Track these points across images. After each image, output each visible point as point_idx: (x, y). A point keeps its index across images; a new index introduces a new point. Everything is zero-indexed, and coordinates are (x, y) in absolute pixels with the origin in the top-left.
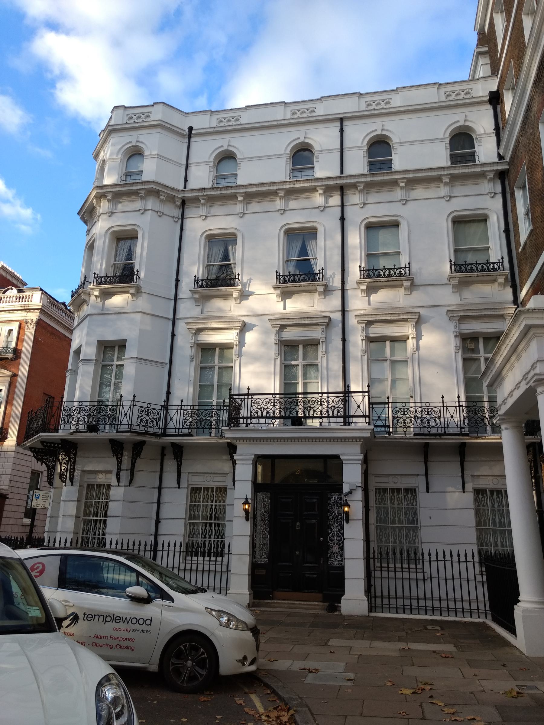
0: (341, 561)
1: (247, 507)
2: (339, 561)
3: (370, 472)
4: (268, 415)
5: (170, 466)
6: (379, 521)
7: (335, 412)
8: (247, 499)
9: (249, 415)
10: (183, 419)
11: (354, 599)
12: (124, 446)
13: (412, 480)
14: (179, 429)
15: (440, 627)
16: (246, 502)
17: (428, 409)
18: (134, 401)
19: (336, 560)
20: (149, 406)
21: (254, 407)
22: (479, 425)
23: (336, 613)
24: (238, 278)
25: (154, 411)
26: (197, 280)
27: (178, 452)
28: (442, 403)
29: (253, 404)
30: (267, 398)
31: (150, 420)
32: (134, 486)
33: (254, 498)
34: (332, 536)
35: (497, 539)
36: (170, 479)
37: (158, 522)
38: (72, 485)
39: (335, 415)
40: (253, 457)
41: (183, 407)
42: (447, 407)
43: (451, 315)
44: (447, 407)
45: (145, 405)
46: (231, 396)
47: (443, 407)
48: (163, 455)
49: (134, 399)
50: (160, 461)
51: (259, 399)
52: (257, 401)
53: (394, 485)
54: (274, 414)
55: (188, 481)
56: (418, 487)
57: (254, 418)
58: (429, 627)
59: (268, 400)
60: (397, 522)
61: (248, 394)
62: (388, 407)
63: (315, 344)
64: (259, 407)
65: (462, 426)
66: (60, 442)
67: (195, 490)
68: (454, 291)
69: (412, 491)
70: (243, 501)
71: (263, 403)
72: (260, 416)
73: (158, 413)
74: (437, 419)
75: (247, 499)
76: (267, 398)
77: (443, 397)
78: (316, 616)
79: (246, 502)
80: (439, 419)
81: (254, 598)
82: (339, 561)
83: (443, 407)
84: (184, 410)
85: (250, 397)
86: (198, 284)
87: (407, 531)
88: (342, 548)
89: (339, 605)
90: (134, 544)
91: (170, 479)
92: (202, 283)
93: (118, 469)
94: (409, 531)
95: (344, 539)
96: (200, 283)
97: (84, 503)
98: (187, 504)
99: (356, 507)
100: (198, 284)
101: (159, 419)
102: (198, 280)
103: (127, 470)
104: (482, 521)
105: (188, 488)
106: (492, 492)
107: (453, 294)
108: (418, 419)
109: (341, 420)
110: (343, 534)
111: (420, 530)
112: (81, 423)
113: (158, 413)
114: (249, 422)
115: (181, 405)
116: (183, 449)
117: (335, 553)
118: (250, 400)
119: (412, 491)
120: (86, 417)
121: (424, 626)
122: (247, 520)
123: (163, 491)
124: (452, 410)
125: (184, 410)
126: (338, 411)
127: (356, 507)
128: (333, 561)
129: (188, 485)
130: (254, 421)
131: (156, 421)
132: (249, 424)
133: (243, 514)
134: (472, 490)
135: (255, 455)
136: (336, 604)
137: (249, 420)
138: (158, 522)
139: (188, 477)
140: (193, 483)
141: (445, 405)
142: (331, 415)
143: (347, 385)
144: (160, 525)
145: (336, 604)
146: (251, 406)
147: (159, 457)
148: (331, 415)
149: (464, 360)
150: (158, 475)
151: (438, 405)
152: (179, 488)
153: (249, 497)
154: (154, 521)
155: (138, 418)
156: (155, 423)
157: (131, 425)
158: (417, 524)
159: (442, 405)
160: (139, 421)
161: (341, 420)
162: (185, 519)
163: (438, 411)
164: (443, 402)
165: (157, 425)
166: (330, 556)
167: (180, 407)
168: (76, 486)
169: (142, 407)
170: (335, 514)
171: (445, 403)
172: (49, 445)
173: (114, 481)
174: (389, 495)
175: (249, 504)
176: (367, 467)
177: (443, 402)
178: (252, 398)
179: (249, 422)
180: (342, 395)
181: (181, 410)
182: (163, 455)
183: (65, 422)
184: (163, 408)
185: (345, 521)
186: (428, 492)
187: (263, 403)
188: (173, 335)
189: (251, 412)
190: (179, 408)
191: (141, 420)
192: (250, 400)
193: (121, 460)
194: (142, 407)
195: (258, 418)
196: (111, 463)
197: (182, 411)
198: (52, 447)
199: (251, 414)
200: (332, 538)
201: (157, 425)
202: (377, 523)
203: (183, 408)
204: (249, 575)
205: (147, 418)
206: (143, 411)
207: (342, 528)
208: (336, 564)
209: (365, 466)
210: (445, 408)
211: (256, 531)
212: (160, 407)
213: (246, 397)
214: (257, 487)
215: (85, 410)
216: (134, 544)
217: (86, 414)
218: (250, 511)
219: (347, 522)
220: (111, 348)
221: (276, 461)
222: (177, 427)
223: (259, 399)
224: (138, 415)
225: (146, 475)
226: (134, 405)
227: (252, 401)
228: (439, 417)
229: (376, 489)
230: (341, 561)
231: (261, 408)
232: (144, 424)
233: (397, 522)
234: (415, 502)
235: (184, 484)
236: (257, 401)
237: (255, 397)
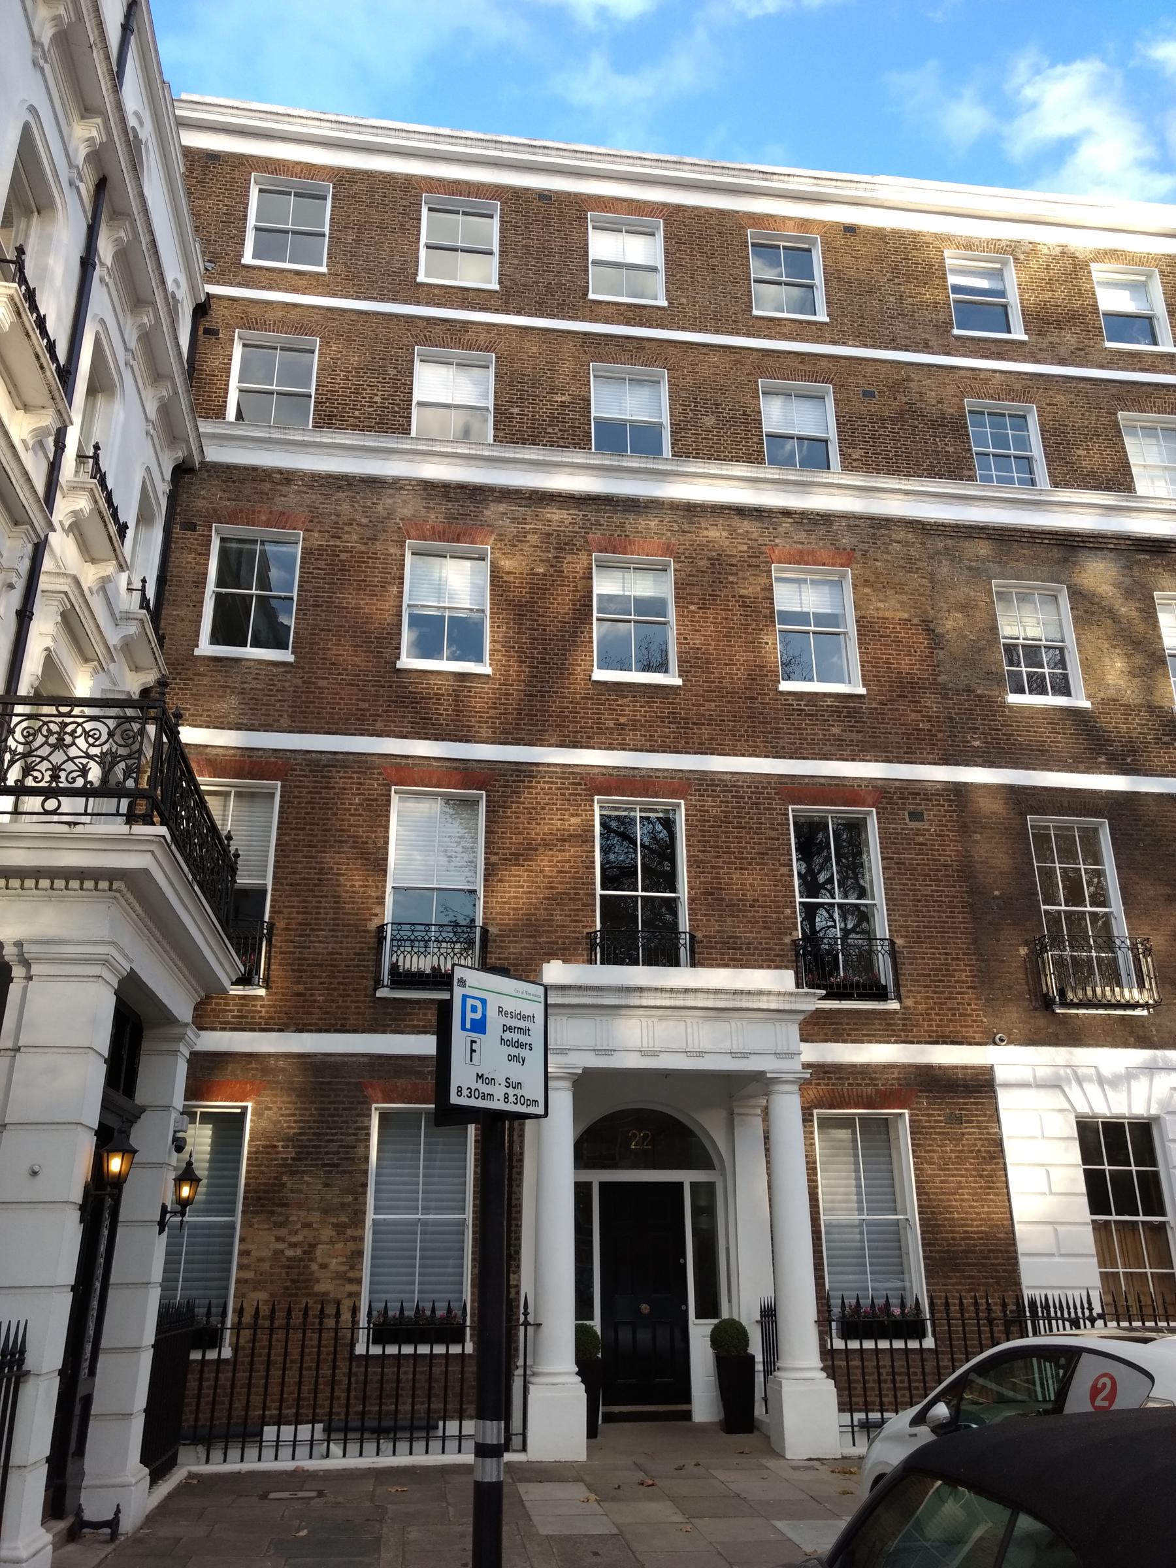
4: (29, 782)
54: (55, 777)
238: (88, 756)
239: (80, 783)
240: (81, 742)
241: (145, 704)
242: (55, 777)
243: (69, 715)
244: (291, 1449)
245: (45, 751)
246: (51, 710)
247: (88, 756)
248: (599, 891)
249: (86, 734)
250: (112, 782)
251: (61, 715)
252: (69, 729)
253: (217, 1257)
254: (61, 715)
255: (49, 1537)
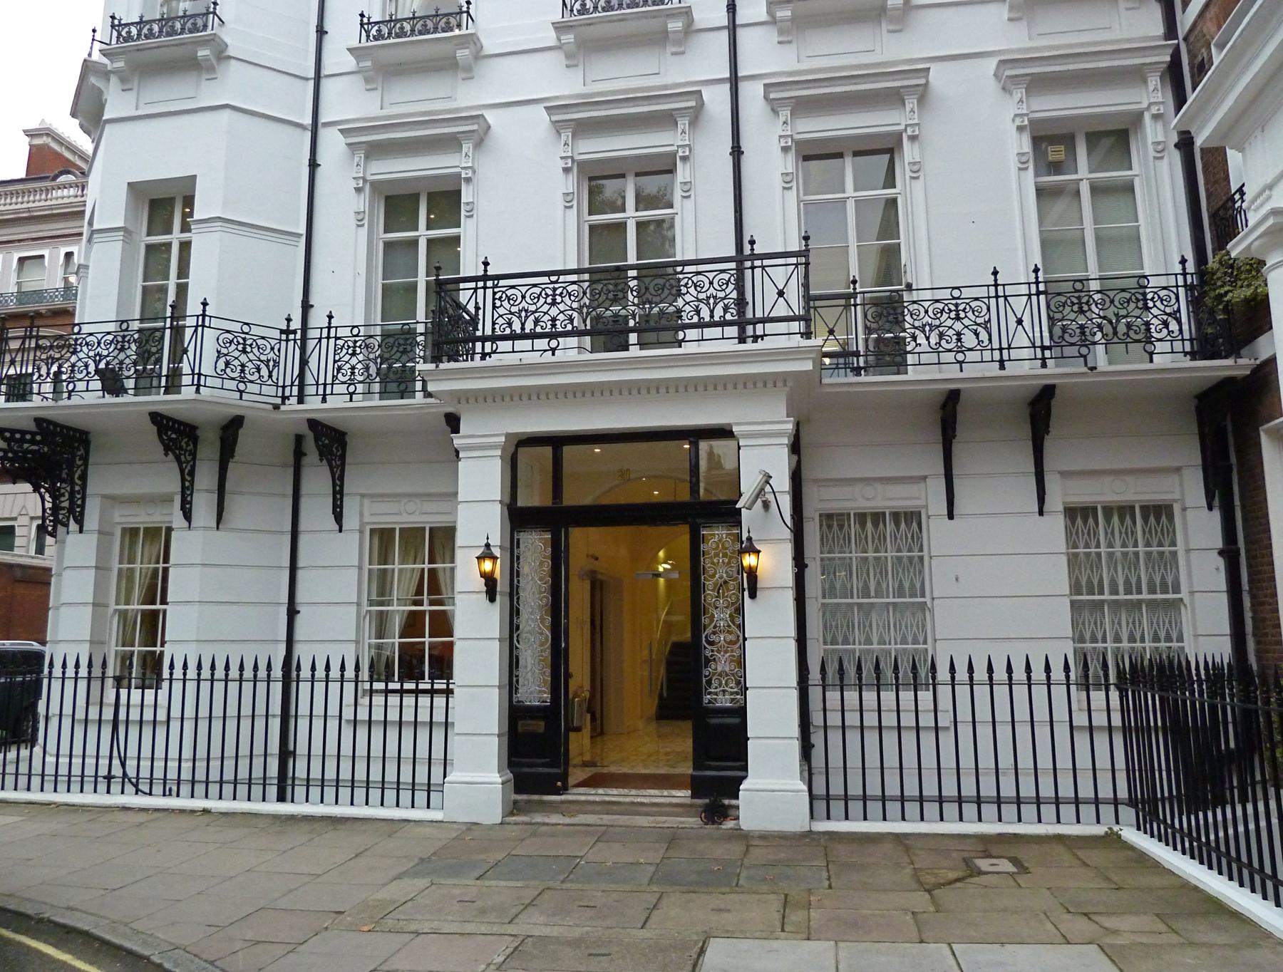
0: (737, 693)
1: (487, 566)
2: (732, 693)
3: (806, 475)
4: (538, 329)
5: (317, 481)
6: (829, 591)
7: (719, 312)
8: (488, 546)
9: (488, 332)
10: (335, 362)
11: (772, 788)
12: (199, 433)
13: (912, 490)
14: (325, 385)
15: (1015, 861)
16: (487, 554)
17: (957, 305)
18: (204, 315)
19: (724, 691)
20: (246, 329)
21: (501, 311)
22: (1090, 338)
23: (729, 824)
24: (468, 12)
25: (260, 342)
26: (365, 23)
27: (329, 443)
28: (992, 289)
29: (498, 303)
30: (535, 285)
31: (250, 365)
32: (226, 530)
33: (513, 547)
34: (714, 633)
35: (1120, 624)
36: (316, 510)
37: (292, 612)
38: (81, 531)
39: (716, 318)
40: (503, 439)
41: (333, 331)
42: (1005, 297)
43: (1008, 73)
44: (1005, 297)
45: (236, 327)
46: (443, 290)
47: (997, 297)
48: (299, 454)
49: (204, 310)
50: (292, 470)
51: (513, 287)
52: (509, 293)
53: (868, 504)
54: (554, 326)
55: (361, 515)
56: (926, 507)
57: (504, 338)
58: (984, 864)
59: (537, 290)
60: (873, 594)
61: (485, 278)
62: (855, 305)
63: (665, 166)
64: (514, 309)
65: (1047, 343)
66: (32, 426)
67: (383, 537)
68: (1013, 15)
69: (911, 518)
70: (479, 552)
71: (523, 297)
72: (519, 331)
73: (272, 349)
74: (980, 329)
75: (488, 546)
76: (535, 285)
77: (995, 273)
78: (672, 839)
79: (487, 554)
80: (986, 328)
81: (518, 790)
82: (732, 693)
83: (997, 297)
84: (337, 338)
85: (490, 284)
86: (368, 32)
87: (898, 615)
88: (741, 662)
89: (734, 802)
90: (213, 667)
91: (316, 510)
92: (379, 31)
93: (184, 488)
94: (868, 614)
95: (745, 639)
96: (374, 32)
97: (115, 572)
98: (360, 568)
99: (772, 562)
100: (368, 32)
101: (276, 364)
102: (369, 23)
103: (207, 491)
104: (1096, 584)
105: (361, 532)
106: (1108, 511)
107: (1012, 24)
108: (931, 330)
109: (733, 331)
110: (742, 627)
111: (932, 611)
112: (79, 376)
113: (272, 349)
114: (488, 350)
115: (329, 328)
116: (348, 439)
117: (720, 675)
118: (489, 292)
119: (911, 518)
120: (91, 362)
121: (964, 860)
122: (492, 599)
123: (303, 540)
124: (1019, 304)
125: (337, 338)
126: (726, 309)
127: (772, 562)
128: (716, 694)
129: (362, 524)
130: (504, 345)
131: (268, 366)
132: (489, 354)
133: (480, 584)
134: (1061, 509)
135: (508, 435)
136: (726, 802)
137: (488, 345)
138: (292, 612)
139: (362, 505)
140: (374, 519)
141: (1001, 293)
142: (707, 319)
143: (746, 239)
144: (300, 620)
145: (726, 802)
146: (494, 307)
147: (291, 460)
148: (707, 319)
149: (1041, 192)
150: (290, 501)
151: (982, 292)
152: (340, 531)
153: (495, 540)
154: (284, 609)
155: (218, 357)
156: (264, 372)
157: (200, 374)
158: (923, 595)
159: (992, 293)
160: (221, 364)
161: (733, 331)
162: (359, 604)
163: (985, 308)
164: (996, 285)
165: (270, 376)
166: (709, 683)
167: (325, 331)
168: (90, 532)
169: (228, 332)
170: (721, 577)
171: (1000, 288)
172: (18, 436)
173: (178, 520)
174: (854, 528)
175: (494, 558)
176: (799, 462)
177: (996, 285)
178: (496, 286)
179: (488, 350)
180: (733, 265)
181: (328, 338)
182: (299, 454)
183: (40, 375)
184: (284, 337)
185: (746, 593)
186: (951, 516)
187: (523, 297)
188: (313, 165)
189: (494, 323)
190: (325, 334)
191: (227, 364)
192: (489, 292)
193: (193, 467)
194: (228, 332)
195: (513, 337)
196: (167, 480)
197: (332, 341)
198: (27, 442)
199: (494, 329)
200: (713, 638)
201: (270, 376)
202: (824, 597)
203: (332, 334)
204: (499, 736)
205: (243, 358)
206: (231, 342)
207: (740, 610)
208: (724, 701)
209: (795, 458)
210: (1001, 300)
211: (518, 628)
212: (276, 334)
213: (481, 284)
214: (519, 518)
215: (87, 344)
216: (213, 667)
217: (91, 354)
218: (497, 575)
219: (753, 596)
220: (164, 204)
221: (567, 450)
222: (322, 381)
223: (513, 287)
224: (218, 352)
225: (261, 508)
226: (203, 326)
227: (494, 293)
228: (986, 325)
229: (821, 515)
230: (737, 693)
231: (520, 311)
232: (236, 375)
233: (873, 594)
234: (917, 540)
235: (350, 520)
236: (509, 293)
237: (502, 283)
238: (511, 313)
239: (508, 331)
240: (692, 290)
241: (739, 258)
242: (554, 326)
243: (556, 282)
244: (404, 719)
245: (545, 308)
246: (545, 279)
247: (511, 313)
248: (128, 398)
249: (509, 299)
250: (527, 331)
251: (552, 282)
252: (558, 292)
253: (1250, 807)
254: (552, 282)
255: (500, 780)
